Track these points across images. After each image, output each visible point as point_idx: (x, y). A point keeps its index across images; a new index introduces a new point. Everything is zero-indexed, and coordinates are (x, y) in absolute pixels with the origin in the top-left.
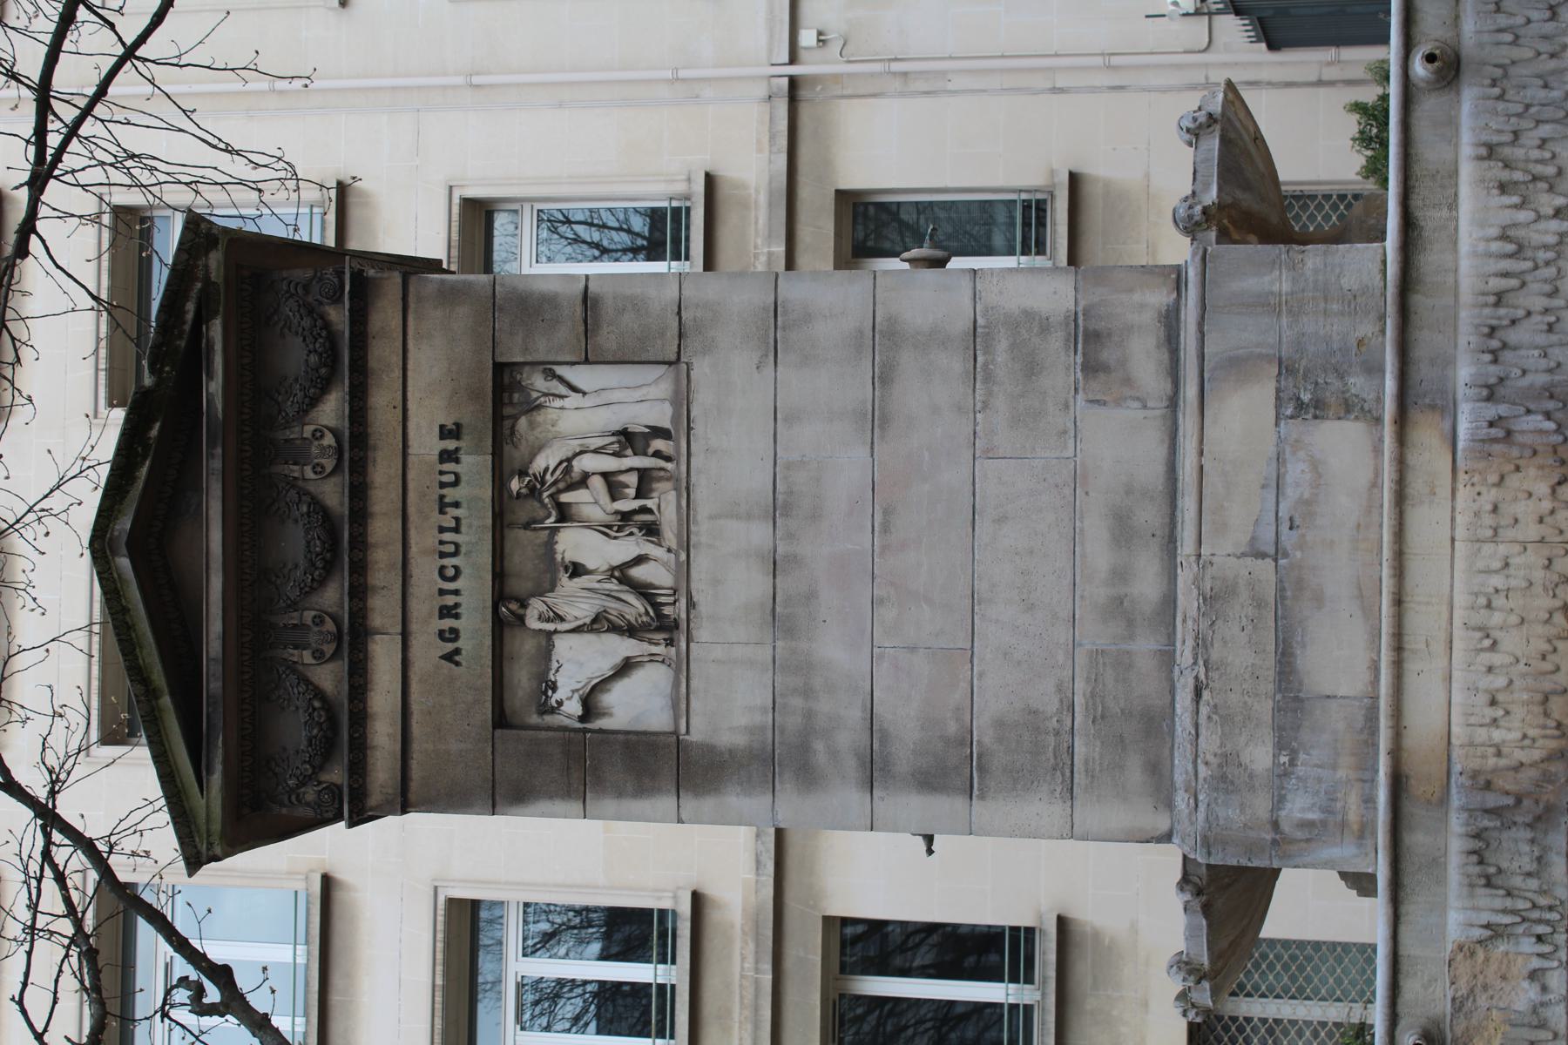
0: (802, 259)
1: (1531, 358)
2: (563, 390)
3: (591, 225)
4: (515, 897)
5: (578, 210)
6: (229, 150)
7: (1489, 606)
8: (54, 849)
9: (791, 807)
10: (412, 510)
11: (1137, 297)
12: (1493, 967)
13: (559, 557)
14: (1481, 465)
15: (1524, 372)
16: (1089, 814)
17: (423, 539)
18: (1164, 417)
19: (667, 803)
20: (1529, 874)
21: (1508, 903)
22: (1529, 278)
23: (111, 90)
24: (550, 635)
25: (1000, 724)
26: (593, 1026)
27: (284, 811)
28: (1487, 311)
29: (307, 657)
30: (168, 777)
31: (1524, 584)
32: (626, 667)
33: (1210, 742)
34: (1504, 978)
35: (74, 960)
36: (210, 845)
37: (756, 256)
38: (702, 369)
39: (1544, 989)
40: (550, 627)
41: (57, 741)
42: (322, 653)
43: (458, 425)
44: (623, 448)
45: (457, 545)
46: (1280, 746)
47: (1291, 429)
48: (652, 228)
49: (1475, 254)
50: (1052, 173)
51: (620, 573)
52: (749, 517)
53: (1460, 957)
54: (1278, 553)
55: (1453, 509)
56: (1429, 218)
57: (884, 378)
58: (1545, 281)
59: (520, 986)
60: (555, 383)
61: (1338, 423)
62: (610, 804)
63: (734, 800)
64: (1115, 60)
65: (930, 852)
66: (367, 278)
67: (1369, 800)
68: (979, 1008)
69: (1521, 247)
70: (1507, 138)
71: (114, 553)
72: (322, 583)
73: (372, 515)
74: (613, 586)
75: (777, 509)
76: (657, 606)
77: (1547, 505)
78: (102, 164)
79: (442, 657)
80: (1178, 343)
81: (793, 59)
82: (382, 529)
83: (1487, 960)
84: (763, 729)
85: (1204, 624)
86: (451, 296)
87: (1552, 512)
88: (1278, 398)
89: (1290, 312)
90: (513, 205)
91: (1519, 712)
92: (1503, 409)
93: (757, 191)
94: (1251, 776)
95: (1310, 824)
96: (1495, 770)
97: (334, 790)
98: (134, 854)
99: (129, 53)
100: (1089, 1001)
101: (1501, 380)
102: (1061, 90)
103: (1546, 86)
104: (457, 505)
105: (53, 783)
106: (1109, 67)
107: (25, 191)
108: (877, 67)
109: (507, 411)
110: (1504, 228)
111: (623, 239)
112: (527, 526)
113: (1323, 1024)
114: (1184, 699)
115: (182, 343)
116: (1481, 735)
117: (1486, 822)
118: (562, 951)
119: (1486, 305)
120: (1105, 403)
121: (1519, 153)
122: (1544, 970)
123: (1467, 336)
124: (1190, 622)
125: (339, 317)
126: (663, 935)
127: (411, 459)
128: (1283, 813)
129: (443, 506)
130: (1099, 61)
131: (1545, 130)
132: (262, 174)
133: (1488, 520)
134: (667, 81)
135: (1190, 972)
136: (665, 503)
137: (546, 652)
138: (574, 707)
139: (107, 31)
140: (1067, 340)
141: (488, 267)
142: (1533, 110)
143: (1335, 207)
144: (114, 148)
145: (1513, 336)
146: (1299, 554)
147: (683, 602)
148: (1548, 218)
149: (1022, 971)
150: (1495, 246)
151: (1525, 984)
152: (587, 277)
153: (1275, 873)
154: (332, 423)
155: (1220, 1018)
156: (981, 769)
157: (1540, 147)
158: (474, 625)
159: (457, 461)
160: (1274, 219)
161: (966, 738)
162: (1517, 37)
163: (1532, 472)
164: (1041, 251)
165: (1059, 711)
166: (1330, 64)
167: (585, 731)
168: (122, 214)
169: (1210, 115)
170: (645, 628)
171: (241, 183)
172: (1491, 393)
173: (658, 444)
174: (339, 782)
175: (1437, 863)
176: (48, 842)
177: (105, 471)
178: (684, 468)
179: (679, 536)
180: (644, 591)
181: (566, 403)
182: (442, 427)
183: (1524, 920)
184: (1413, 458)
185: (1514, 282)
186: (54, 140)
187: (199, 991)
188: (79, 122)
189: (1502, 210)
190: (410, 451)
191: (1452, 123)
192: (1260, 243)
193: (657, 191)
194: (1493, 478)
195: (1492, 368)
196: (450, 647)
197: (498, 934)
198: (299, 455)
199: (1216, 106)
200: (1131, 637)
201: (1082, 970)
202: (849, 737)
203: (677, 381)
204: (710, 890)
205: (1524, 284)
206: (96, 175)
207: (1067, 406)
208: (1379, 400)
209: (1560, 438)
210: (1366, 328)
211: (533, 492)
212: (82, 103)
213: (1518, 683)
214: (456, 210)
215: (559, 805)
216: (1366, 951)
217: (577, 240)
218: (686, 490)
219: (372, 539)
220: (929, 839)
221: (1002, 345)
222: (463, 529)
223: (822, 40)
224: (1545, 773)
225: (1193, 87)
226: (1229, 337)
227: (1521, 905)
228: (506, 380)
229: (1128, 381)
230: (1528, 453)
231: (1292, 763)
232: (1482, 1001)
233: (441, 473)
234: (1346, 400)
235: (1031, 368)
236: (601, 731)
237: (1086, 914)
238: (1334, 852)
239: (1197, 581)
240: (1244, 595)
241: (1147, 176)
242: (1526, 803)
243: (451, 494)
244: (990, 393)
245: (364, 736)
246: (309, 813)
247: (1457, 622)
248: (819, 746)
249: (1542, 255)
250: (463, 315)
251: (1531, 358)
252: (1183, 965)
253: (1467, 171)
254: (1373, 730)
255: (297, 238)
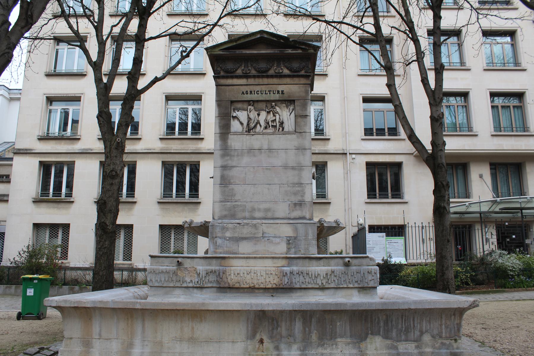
0: (315, 156)
1: (297, 280)
2: (290, 112)
3: (321, 119)
4: (202, 107)
5: (323, 116)
6: (332, 54)
7: (255, 273)
8: (209, 26)
9: (218, 153)
10: (269, 86)
11: (308, 212)
12: (193, 274)
13: (261, 112)
14: (279, 272)
15: (295, 278)
16: (217, 205)
17: (264, 88)
18: (287, 217)
19: (218, 131)
20: (209, 280)
21: (204, 277)
22: (311, 279)
23: (342, 34)
24: (247, 110)
25: (233, 189)
26: (180, 122)
27: (216, 65)
28: (305, 272)
29: (243, 68)
30: (222, 44)
31: (258, 279)
32: (242, 124)
33: (230, 226)
34: (191, 276)
35: (190, 30)
36: (210, 52)
37: (316, 148)
38: (294, 136)
39: (189, 283)
40: (249, 110)
41: (228, 26)
42: (243, 71)
43: (284, 94)
44: (280, 123)
45: (263, 94)
46: (230, 238)
47: (285, 239)
48: (320, 130)
49: (315, 270)
50: (331, 199)
51: (258, 122)
52: (268, 145)
53: (194, 269)
54: (263, 237)
55: (271, 267)
56: (322, 262)
57: (293, 168)
58: (311, 282)
59: (187, 108)
60: (292, 111)
61: (286, 247)
62: (218, 121)
63: (219, 143)
64: (350, 210)
65: (210, 178)
66: (309, 78)
67: (221, 253)
68: (185, 189)
69: (316, 277)
70: (335, 275)
71: (261, 34)
72: (256, 70)
73: (268, 79)
74: (256, 121)
75: (270, 150)
76: (252, 129)
77: (272, 282)
78: (329, 33)
79: (243, 92)
80: (300, 219)
81: (350, 154)
82: (265, 81)
83: (194, 273)
84: (231, 148)
85: (251, 225)
86: (307, 92)
87: (271, 283)
88: (290, 237)
89: (305, 239)
90: (324, 105)
91: (236, 278)
92: (289, 275)
93: (327, 148)
94: (224, 233)
95: (216, 243)
96: (226, 274)
97: (219, 73)
98: (209, 40)
99: (348, 37)
100: (186, 207)
101: (294, 275)
102: (345, 201)
103: (344, 281)
104: (270, 94)
105: (221, 26)
106: (349, 209)
107: (324, 19)
108: (349, 168)
109: (286, 102)
110: (320, 274)
111: (318, 125)
112: (266, 106)
113: (183, 248)
114: (238, 221)
115: (297, 45)
116: (232, 272)
117: (217, 273)
118: (193, 116)
119: (306, 272)
120: (289, 207)
121: (333, 277)
122: (192, 283)
123: (301, 269)
124: (251, 222)
125: (303, 73)
126: (196, 133)
127: (278, 85)
128: (218, 238)
129: (269, 91)
130: (350, 207)
131: (336, 281)
132: (328, 60)
133: (270, 273)
134: (346, 132)
135: (190, 223)
136: (271, 130)
137: (244, 110)
138: (234, 115)
139: (352, 33)
140: (300, 200)
141: (312, 100)
142: (340, 279)
143: (325, 248)
144: (332, 35)
145: (301, 276)
146: (263, 241)
147: (253, 134)
148: (322, 282)
149: (191, 196)
150: (317, 273)
151: (190, 280)
152: (310, 116)
153: (208, 238)
154: (284, 72)
155: (184, 230)
156: (225, 186)
157: (334, 280)
158: (249, 97)
159: (278, 94)
160: (321, 236)
161: (230, 183)
162: (352, 276)
163: (278, 280)
164: (317, 197)
165: (235, 200)
166: (349, 246)
167: (230, 117)
168: (321, 37)
169: (339, 224)
170: (249, 127)
171: (326, 57)
172: (291, 273)
173: (281, 129)
174: (221, 74)
175: (210, 265)
176: (211, 25)
177: (276, 33)
178: (277, 133)
179: (265, 133)
180: (255, 127)
181: (288, 113)
182: (283, 91)
183: (201, 279)
184: (280, 260)
185: (310, 276)
186: (333, 24)
187: (185, 52)
188: (336, 29)
189: (323, 274)
190: (279, 85)
191: (338, 265)
192: (317, 233)
193: (327, 130)
194: (277, 274)
195: (296, 273)
196: (245, 93)
197: (196, 104)
198: (278, 66)
199: (341, 225)
200: (248, 212)
201: (191, 206)
202: (230, 163)
203: (292, 132)
204: (204, 141)
205: (310, 278)
206: (327, 32)
207: (288, 200)
208: (290, 254)
209: (284, 285)
210: (302, 252)
211: (272, 107)
212: (340, 29)
213: (241, 278)
214: (323, 95)
215: (217, 112)
216: (196, 252)
217: (318, 117)
218: (273, 134)
219: (263, 79)
220: (212, 178)
221: (299, 189)
222: (266, 95)
223: (353, 159)
224: (226, 283)
225: (345, 223)
226: (301, 229)
227: (203, 279)
228: (292, 102)
229: (293, 211)
230: (281, 279)
231: (227, 240)
232: (187, 272)
233: (275, 91)
234: (290, 248)
235: (295, 194)
236: (230, 119)
237: (201, 207)
238: (212, 247)
239: (258, 223)
240: (256, 231)
241: (330, 216)
242: (221, 280)
243: (272, 93)
244: (291, 187)
245: (229, 78)
246: (215, 69)
247: (252, 268)
248: (228, 158)
249: (315, 281)
250: (303, 94)
251: (297, 280)
252: (192, 222)
253: (330, 268)
254: (233, 254)
255: (316, 66)
